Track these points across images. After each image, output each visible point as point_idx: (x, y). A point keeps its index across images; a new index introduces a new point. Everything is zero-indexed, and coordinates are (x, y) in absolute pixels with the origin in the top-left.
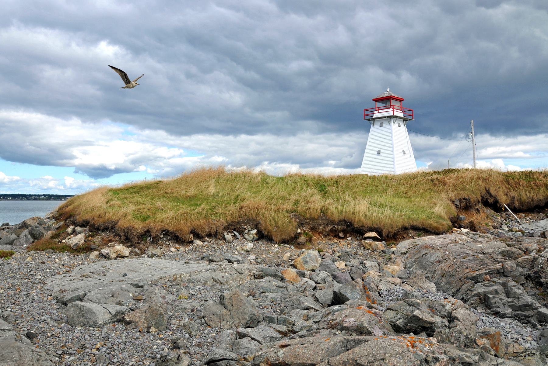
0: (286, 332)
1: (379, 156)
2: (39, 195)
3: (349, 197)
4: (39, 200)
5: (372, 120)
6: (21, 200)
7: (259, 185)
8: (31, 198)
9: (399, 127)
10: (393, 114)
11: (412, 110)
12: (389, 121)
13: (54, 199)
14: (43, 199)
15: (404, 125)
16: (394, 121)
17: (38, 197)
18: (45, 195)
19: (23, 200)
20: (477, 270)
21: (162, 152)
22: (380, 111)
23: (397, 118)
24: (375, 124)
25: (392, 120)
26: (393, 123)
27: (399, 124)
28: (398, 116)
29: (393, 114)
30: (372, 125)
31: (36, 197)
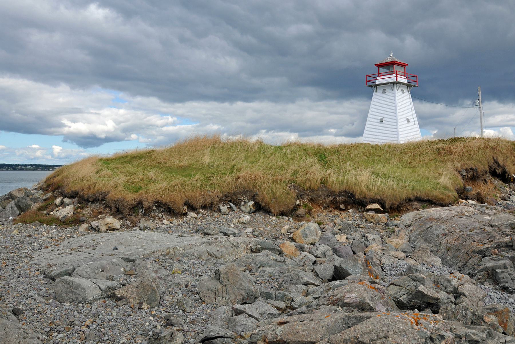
1: (382, 124)
2: (26, 165)
3: (350, 167)
4: (26, 170)
6: (7, 170)
8: (18, 168)
9: (403, 94)
12: (392, 87)
13: (42, 169)
14: (30, 169)
15: (408, 92)
16: (398, 88)
17: (25, 167)
18: (32, 165)
19: (9, 170)
20: (484, 244)
21: (156, 120)
23: (400, 84)
25: (395, 86)
26: (396, 90)
31: (23, 167)
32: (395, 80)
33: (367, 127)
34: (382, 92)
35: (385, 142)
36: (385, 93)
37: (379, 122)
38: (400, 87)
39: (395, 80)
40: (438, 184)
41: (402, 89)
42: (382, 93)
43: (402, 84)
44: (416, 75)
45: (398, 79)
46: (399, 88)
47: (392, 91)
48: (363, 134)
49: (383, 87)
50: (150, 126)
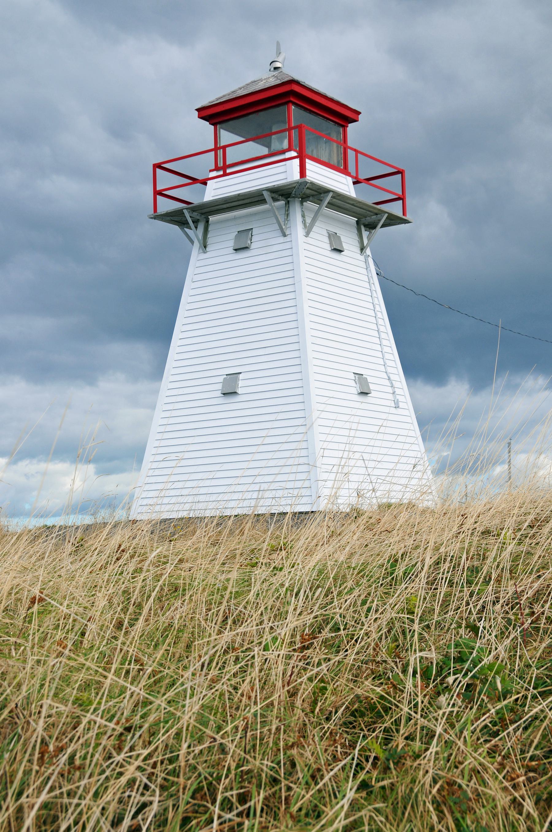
0: (100, 739)
1: (232, 403)
3: (63, 559)
5: (196, 222)
7: (434, 717)
9: (335, 255)
10: (303, 172)
11: (400, 172)
12: (281, 219)
15: (362, 249)
16: (308, 220)
22: (228, 171)
23: (319, 201)
24: (209, 241)
25: (296, 211)
26: (300, 230)
27: (333, 237)
28: (327, 191)
29: (303, 172)
30: (197, 244)
32: (296, 176)
33: (180, 343)
34: (231, 243)
35: (246, 503)
36: (246, 248)
37: (219, 394)
38: (320, 218)
39: (296, 176)
40: (406, 760)
41: (333, 230)
42: (231, 250)
43: (331, 205)
44: (401, 167)
45: (308, 173)
46: (314, 220)
47: (282, 239)
48: (159, 392)
49: (235, 218)
50: (68, 629)
